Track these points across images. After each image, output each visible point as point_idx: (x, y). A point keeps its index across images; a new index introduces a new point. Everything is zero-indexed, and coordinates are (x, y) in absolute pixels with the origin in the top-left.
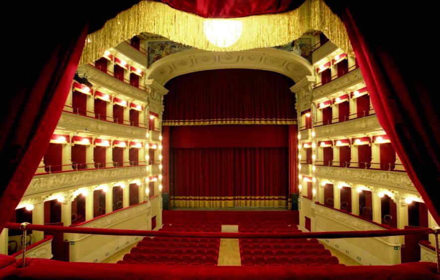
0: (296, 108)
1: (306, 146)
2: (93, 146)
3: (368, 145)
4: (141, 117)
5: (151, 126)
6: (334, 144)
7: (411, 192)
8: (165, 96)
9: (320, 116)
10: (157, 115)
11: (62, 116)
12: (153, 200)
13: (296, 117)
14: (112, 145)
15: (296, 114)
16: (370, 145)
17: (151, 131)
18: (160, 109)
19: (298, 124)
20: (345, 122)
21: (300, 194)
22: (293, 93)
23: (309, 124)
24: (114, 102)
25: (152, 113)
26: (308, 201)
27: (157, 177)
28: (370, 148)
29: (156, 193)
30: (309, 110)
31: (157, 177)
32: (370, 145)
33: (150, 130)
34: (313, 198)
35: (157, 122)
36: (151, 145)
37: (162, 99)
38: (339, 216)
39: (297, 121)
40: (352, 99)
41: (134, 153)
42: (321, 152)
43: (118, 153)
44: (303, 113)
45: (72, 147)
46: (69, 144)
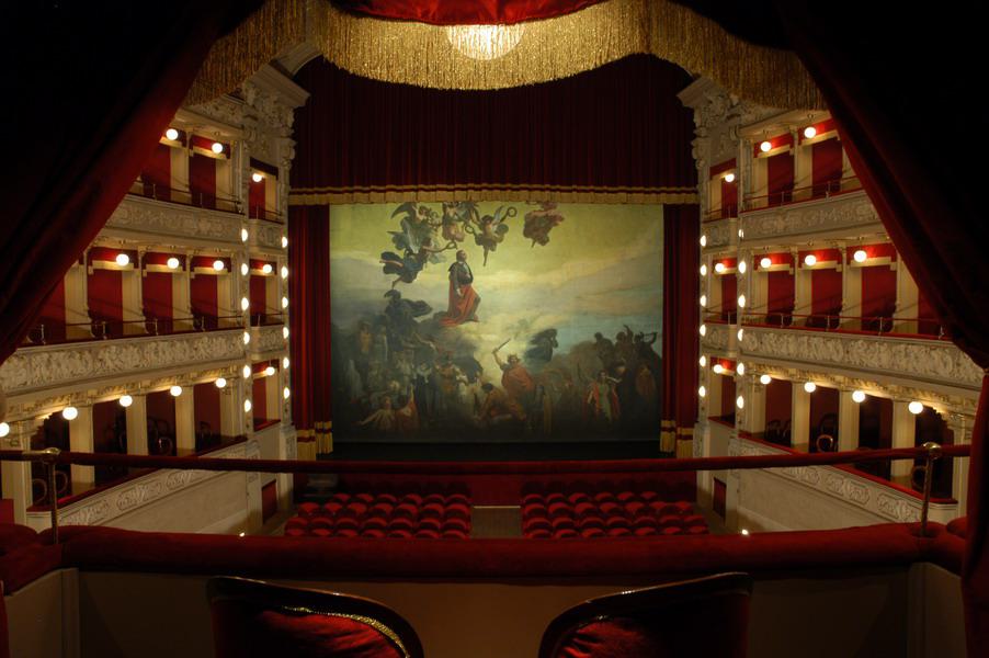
0: (695, 157)
1: (721, 269)
2: (189, 276)
3: (889, 266)
4: (223, 178)
5: (257, 210)
6: (845, 261)
7: (868, 375)
8: (298, 112)
9: (761, 176)
10: (271, 170)
11: (122, 204)
12: (262, 434)
13: (696, 182)
14: (188, 267)
15: (696, 172)
16: (791, 273)
17: (255, 221)
18: (283, 152)
19: (703, 202)
20: (828, 199)
21: (701, 413)
22: (688, 108)
23: (731, 204)
24: (191, 148)
25: (257, 165)
26: (722, 429)
27: (276, 364)
28: (792, 278)
29: (271, 415)
30: (730, 165)
31: (276, 364)
32: (838, 270)
33: (252, 216)
34: (738, 419)
35: (276, 198)
36: (254, 264)
37: (290, 120)
38: (847, 485)
39: (696, 192)
40: (800, 147)
41: (205, 288)
42: (762, 289)
43: (157, 288)
44: (717, 170)
45: (192, 280)
46: (138, 271)
